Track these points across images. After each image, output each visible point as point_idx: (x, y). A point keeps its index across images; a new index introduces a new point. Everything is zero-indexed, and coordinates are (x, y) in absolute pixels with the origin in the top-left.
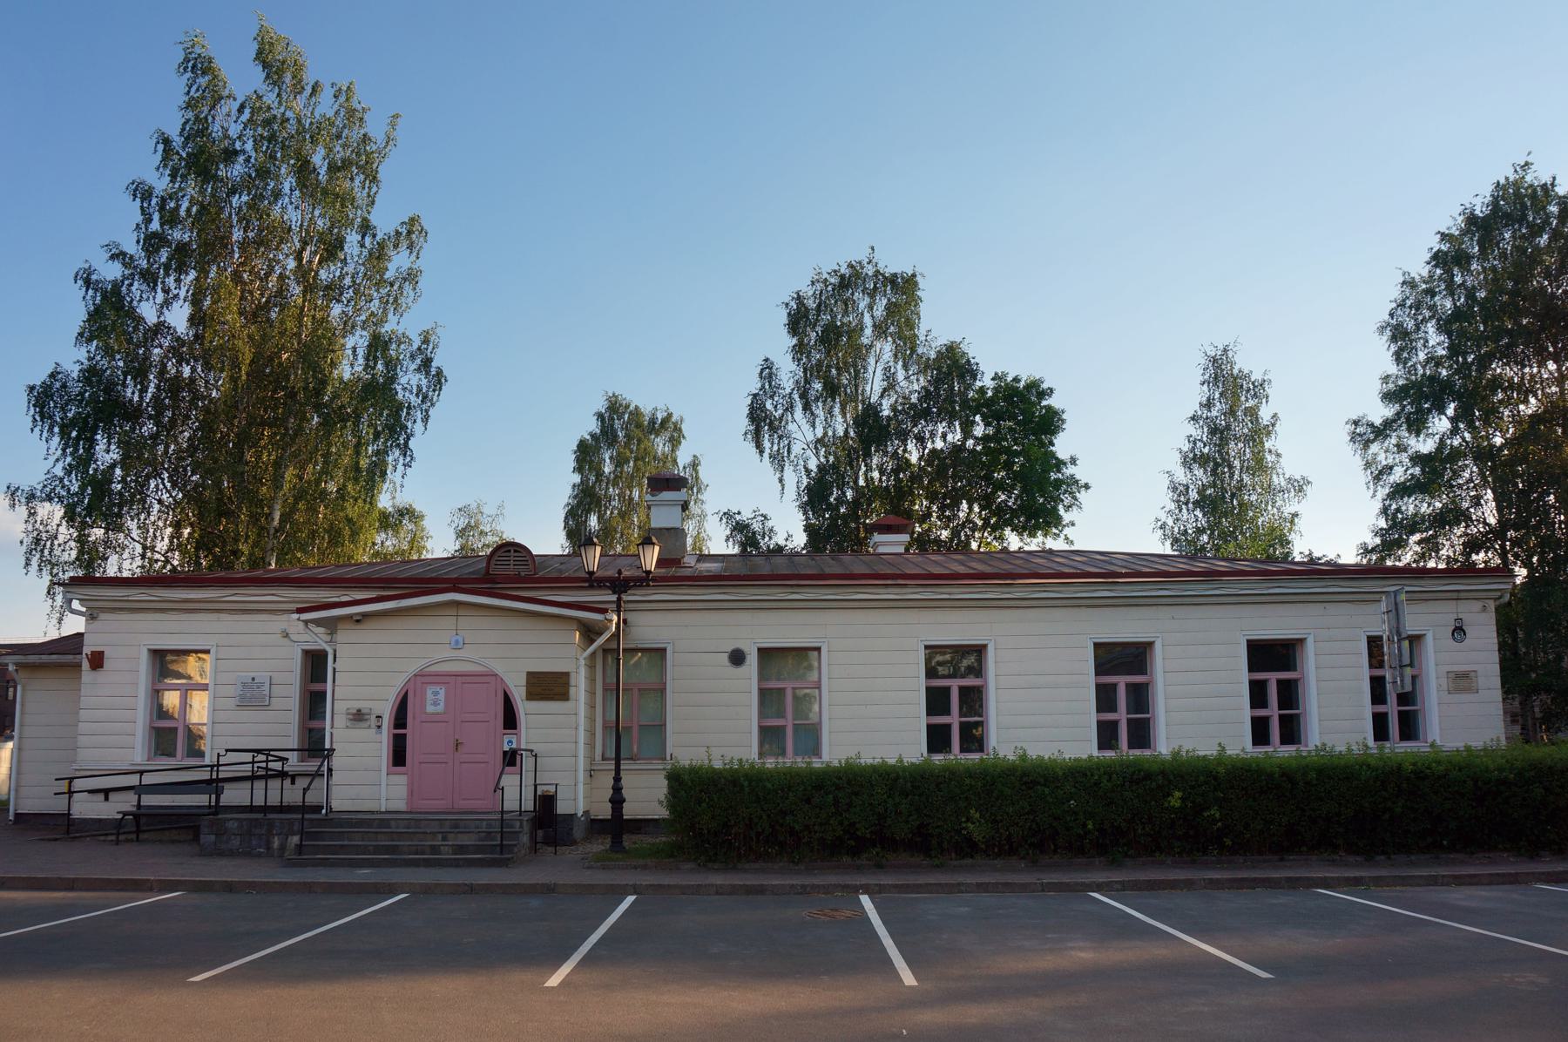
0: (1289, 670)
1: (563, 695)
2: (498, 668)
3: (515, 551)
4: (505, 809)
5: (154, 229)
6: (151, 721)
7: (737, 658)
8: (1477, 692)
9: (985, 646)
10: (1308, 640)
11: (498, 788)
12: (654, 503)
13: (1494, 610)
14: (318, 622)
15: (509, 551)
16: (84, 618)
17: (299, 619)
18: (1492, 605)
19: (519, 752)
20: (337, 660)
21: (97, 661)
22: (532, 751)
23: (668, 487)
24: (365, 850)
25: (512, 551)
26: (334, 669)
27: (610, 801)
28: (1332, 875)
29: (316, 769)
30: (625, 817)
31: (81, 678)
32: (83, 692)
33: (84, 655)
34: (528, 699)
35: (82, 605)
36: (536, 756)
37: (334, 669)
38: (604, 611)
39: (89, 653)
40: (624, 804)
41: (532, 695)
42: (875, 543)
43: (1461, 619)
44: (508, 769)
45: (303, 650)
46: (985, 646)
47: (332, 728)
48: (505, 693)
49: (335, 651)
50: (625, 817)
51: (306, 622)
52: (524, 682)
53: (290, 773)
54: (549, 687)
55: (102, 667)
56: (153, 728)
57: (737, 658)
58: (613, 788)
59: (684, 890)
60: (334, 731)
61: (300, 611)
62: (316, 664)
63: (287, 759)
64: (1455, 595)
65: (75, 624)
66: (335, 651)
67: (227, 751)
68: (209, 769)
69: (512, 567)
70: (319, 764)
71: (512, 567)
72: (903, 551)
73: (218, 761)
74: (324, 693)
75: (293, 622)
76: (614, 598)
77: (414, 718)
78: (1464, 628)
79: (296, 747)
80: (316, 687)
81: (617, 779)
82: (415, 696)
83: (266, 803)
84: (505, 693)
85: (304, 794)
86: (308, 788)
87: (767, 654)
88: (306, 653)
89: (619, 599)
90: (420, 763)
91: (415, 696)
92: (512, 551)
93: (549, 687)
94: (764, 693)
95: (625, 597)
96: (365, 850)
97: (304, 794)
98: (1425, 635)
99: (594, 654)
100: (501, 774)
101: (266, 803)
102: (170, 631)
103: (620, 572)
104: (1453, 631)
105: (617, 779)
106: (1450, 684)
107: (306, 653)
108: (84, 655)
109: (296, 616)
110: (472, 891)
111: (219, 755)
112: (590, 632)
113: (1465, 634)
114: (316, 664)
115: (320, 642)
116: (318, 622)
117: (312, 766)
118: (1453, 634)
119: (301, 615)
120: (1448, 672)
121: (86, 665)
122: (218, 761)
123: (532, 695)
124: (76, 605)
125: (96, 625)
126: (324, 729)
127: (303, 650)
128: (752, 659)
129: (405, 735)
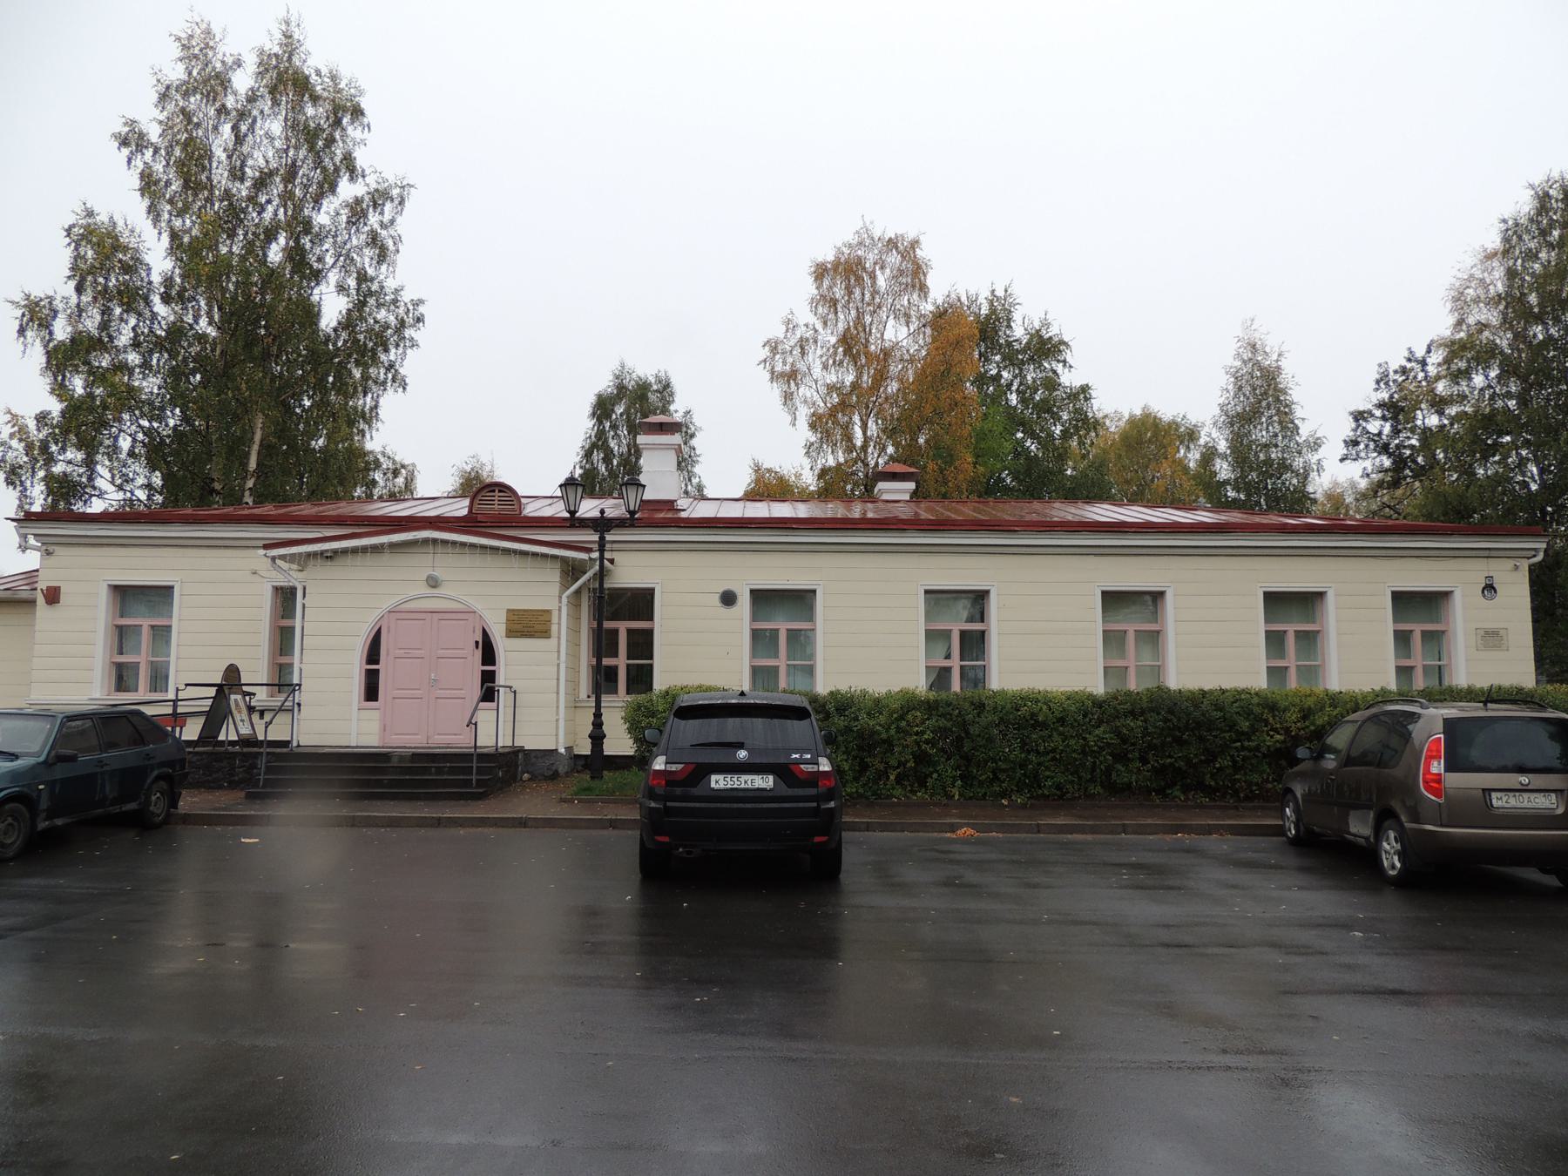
0: (1422, 641)
1: (545, 634)
2: (477, 605)
3: (500, 491)
4: (478, 745)
5: (126, 149)
6: (111, 656)
7: (728, 599)
8: (1508, 650)
9: (987, 592)
10: (1329, 594)
11: (472, 724)
12: (647, 446)
13: (1527, 569)
14: (291, 558)
15: (494, 491)
16: (39, 553)
17: (265, 555)
18: (1525, 565)
19: (496, 689)
20: (307, 595)
21: (53, 596)
22: (511, 687)
23: (662, 430)
24: (445, 783)
25: (497, 491)
26: (304, 605)
27: (590, 736)
28: (495, 816)
29: (279, 704)
30: (605, 753)
31: (35, 614)
32: (37, 628)
33: (39, 591)
34: (508, 636)
35: (37, 541)
36: (515, 692)
37: (304, 605)
38: (589, 550)
39: (44, 588)
40: (604, 740)
41: (511, 633)
42: (880, 490)
43: (1492, 577)
44: (482, 705)
45: (273, 587)
46: (987, 592)
47: (301, 663)
48: (484, 630)
49: (305, 588)
50: (605, 753)
51: (273, 559)
52: (504, 619)
53: (257, 708)
54: (528, 625)
55: (59, 602)
56: (113, 663)
57: (728, 599)
58: (593, 724)
59: (422, 823)
60: (303, 666)
61: (266, 547)
62: (286, 598)
63: (254, 694)
64: (1486, 553)
65: (32, 560)
66: (305, 588)
67: (187, 685)
68: (172, 703)
69: (496, 502)
70: (283, 699)
71: (496, 502)
72: (908, 498)
73: (177, 695)
74: (293, 628)
75: (259, 558)
76: (596, 538)
77: (388, 654)
78: (1494, 585)
79: (265, 682)
80: (286, 623)
81: (598, 715)
82: (389, 631)
83: (266, 737)
84: (484, 630)
85: (266, 727)
86: (271, 722)
87: (762, 598)
88: (277, 589)
89: (602, 538)
90: (394, 698)
91: (389, 631)
92: (497, 491)
93: (528, 625)
94: (756, 635)
95: (608, 537)
96: (445, 783)
97: (266, 727)
98: (1452, 591)
99: (578, 592)
100: (476, 709)
101: (266, 737)
102: (142, 568)
103: (602, 512)
104: (1484, 589)
105: (598, 715)
106: (1479, 642)
107: (277, 589)
108: (39, 591)
109: (262, 552)
110: (439, 824)
111: (177, 690)
112: (572, 571)
113: (1495, 592)
114: (286, 598)
115: (293, 580)
116: (291, 558)
117: (278, 700)
118: (1483, 592)
119: (268, 551)
120: (1476, 629)
121: (40, 600)
122: (177, 695)
123: (511, 633)
124: (32, 541)
125: (52, 560)
126: (293, 664)
127: (273, 587)
128: (744, 601)
129: (378, 671)
